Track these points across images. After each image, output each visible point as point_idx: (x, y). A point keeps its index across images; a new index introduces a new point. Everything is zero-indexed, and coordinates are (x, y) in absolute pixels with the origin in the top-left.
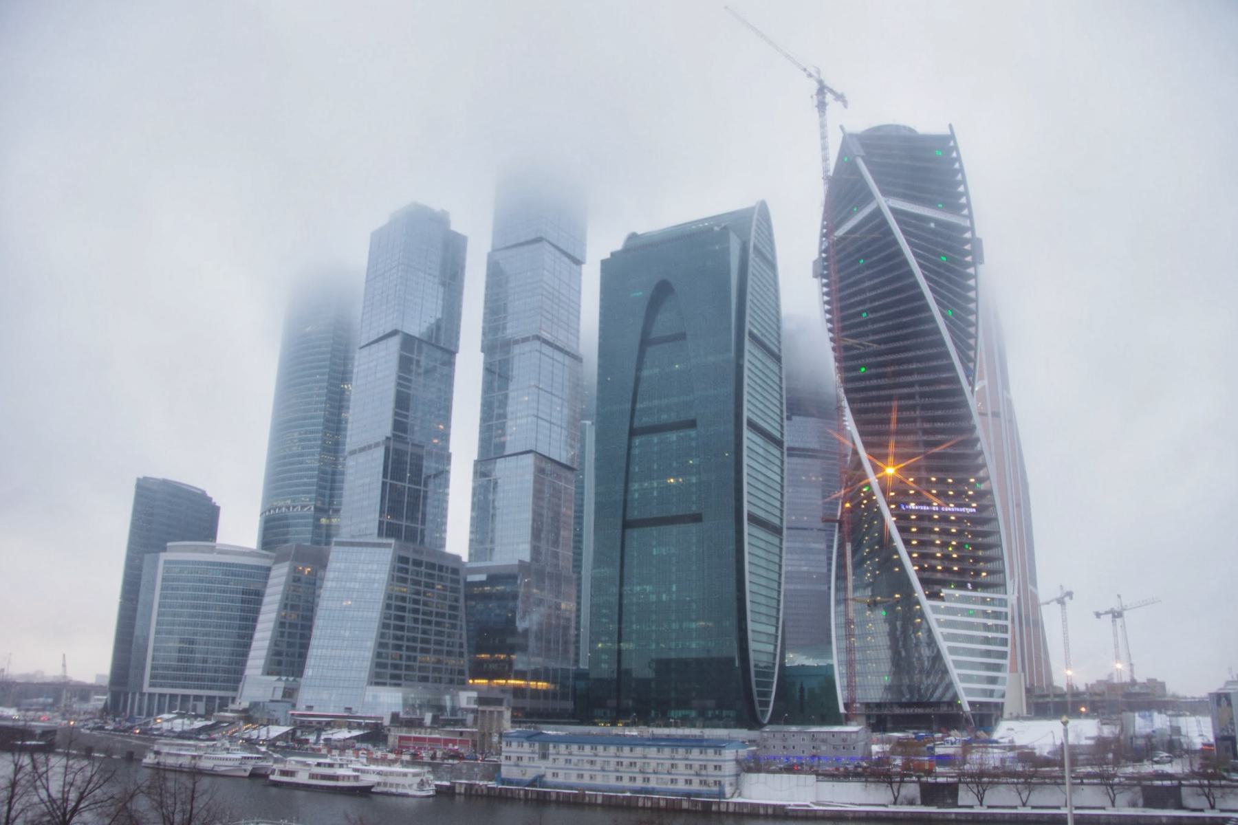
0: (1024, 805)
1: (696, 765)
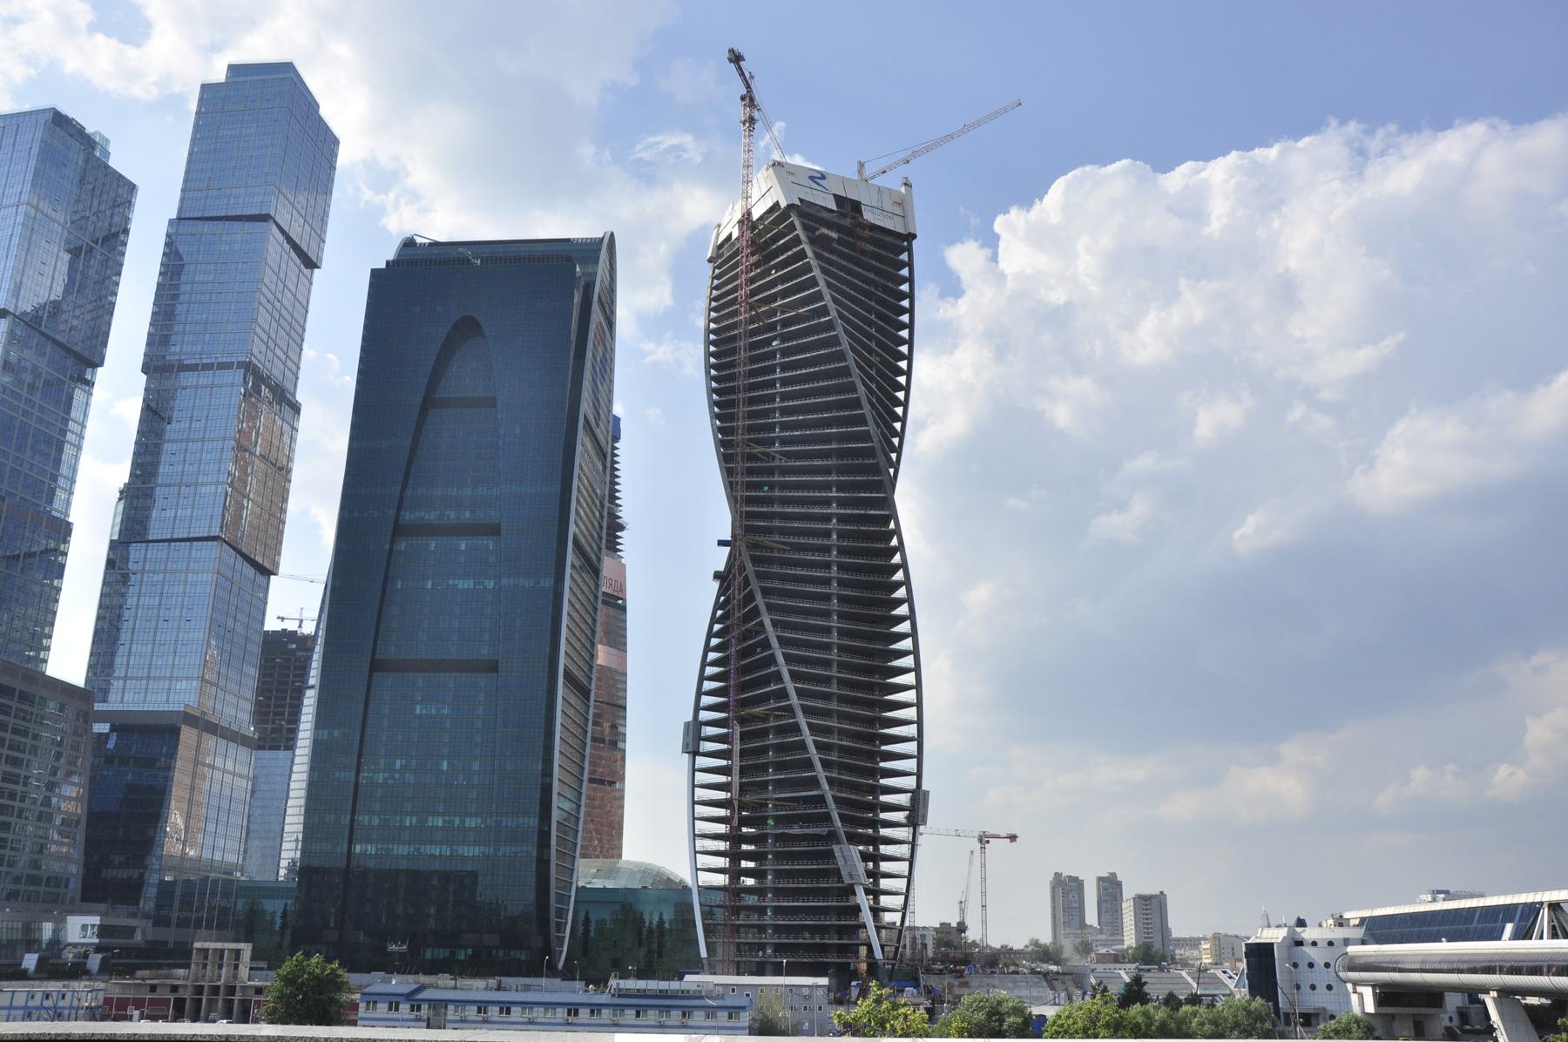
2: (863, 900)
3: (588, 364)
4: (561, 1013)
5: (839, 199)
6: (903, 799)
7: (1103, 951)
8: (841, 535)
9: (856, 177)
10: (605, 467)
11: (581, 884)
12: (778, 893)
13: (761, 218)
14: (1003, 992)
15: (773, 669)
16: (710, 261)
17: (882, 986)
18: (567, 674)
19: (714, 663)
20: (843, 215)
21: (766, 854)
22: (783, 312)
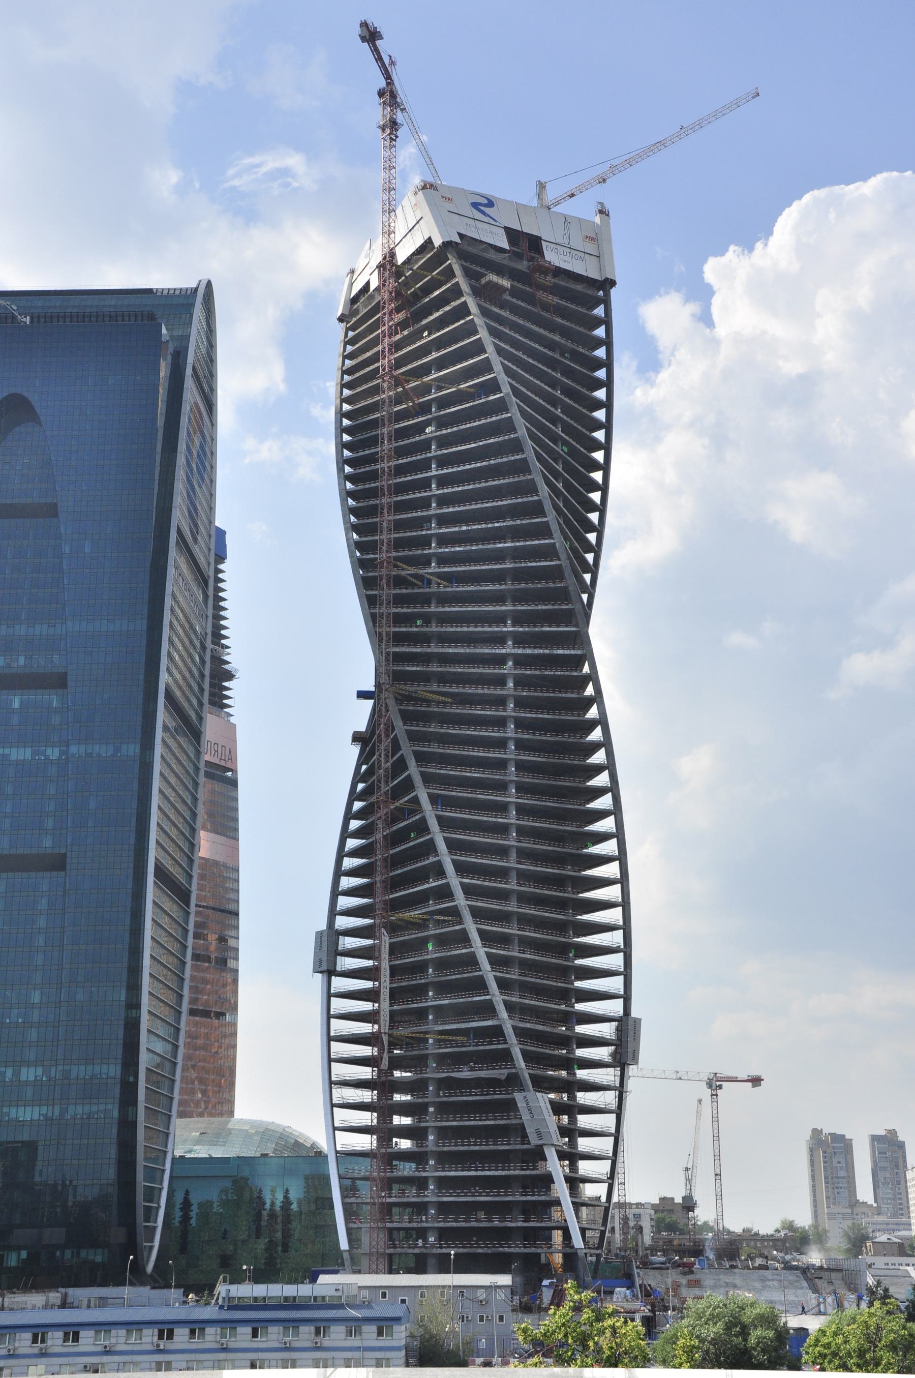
2: (556, 1167)
3: (181, 460)
4: (149, 1336)
5: (513, 235)
6: (606, 1030)
7: (883, 1238)
8: (520, 682)
9: (535, 203)
10: (206, 596)
11: (178, 1153)
12: (445, 1159)
13: (408, 261)
14: (750, 1294)
15: (432, 859)
16: (341, 319)
17: (581, 1286)
18: (160, 871)
19: (354, 853)
20: (518, 256)
21: (425, 1106)
22: (440, 388)
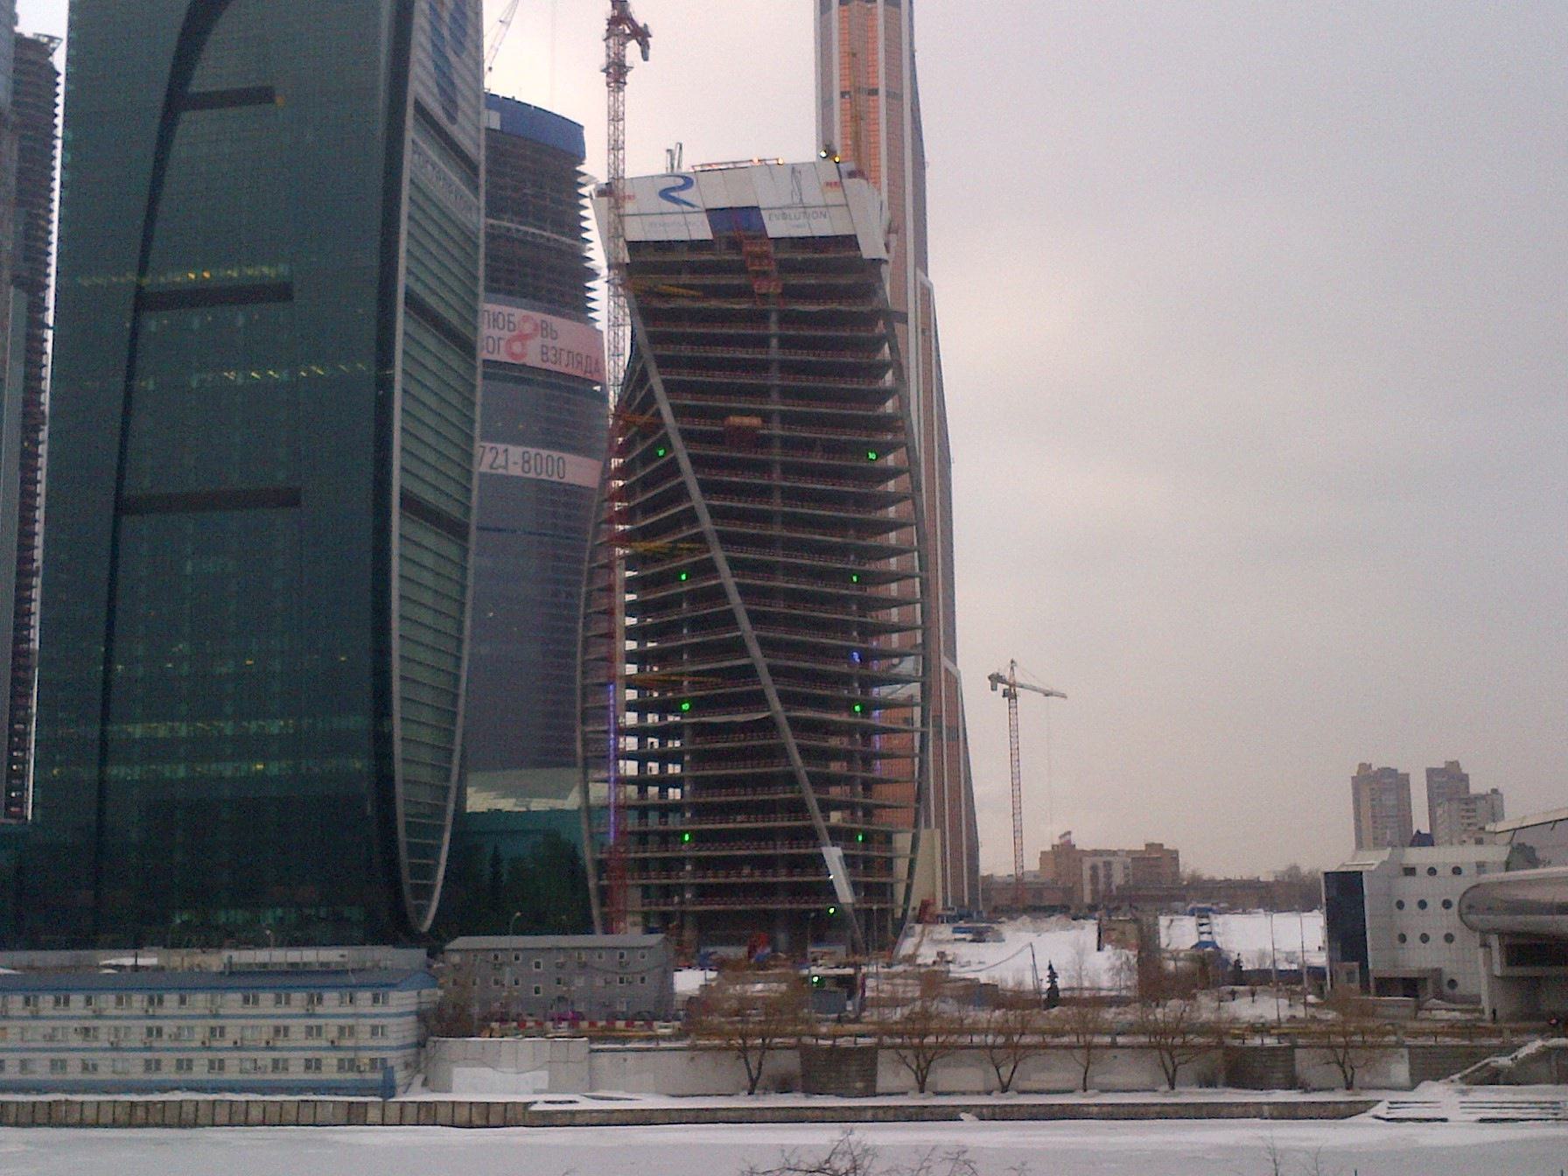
0: (1005, 1089)
1: (331, 1028)
18: (409, 502)
